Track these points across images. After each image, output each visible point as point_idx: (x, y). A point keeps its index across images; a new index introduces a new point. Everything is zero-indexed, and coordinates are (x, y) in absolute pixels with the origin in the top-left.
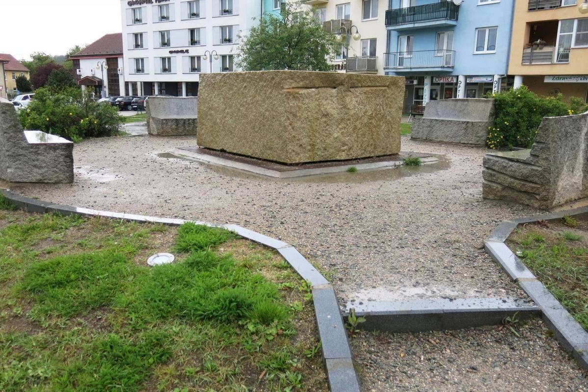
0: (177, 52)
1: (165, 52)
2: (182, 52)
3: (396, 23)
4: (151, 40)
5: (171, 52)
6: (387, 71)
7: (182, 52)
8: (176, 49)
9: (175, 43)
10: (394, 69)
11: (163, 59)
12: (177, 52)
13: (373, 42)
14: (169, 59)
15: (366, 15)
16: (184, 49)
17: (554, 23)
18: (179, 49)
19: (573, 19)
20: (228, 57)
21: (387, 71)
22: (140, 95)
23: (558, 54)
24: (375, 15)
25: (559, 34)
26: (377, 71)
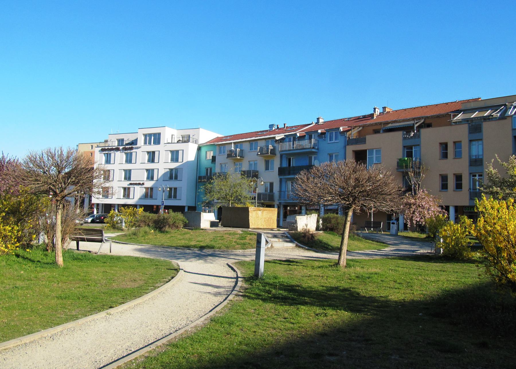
0: (136, 184)
1: (126, 184)
2: (139, 184)
3: (285, 175)
4: (118, 176)
5: (131, 184)
6: (280, 201)
7: (139, 184)
8: (135, 182)
9: (134, 178)
10: (284, 200)
11: (125, 189)
12: (136, 184)
13: (272, 184)
14: (129, 188)
15: (267, 168)
16: (141, 182)
17: (365, 151)
18: (138, 182)
19: (373, 149)
20: (157, 135)
21: (280, 201)
22: (106, 236)
23: (366, 164)
24: (272, 169)
25: (368, 156)
26: (274, 201)
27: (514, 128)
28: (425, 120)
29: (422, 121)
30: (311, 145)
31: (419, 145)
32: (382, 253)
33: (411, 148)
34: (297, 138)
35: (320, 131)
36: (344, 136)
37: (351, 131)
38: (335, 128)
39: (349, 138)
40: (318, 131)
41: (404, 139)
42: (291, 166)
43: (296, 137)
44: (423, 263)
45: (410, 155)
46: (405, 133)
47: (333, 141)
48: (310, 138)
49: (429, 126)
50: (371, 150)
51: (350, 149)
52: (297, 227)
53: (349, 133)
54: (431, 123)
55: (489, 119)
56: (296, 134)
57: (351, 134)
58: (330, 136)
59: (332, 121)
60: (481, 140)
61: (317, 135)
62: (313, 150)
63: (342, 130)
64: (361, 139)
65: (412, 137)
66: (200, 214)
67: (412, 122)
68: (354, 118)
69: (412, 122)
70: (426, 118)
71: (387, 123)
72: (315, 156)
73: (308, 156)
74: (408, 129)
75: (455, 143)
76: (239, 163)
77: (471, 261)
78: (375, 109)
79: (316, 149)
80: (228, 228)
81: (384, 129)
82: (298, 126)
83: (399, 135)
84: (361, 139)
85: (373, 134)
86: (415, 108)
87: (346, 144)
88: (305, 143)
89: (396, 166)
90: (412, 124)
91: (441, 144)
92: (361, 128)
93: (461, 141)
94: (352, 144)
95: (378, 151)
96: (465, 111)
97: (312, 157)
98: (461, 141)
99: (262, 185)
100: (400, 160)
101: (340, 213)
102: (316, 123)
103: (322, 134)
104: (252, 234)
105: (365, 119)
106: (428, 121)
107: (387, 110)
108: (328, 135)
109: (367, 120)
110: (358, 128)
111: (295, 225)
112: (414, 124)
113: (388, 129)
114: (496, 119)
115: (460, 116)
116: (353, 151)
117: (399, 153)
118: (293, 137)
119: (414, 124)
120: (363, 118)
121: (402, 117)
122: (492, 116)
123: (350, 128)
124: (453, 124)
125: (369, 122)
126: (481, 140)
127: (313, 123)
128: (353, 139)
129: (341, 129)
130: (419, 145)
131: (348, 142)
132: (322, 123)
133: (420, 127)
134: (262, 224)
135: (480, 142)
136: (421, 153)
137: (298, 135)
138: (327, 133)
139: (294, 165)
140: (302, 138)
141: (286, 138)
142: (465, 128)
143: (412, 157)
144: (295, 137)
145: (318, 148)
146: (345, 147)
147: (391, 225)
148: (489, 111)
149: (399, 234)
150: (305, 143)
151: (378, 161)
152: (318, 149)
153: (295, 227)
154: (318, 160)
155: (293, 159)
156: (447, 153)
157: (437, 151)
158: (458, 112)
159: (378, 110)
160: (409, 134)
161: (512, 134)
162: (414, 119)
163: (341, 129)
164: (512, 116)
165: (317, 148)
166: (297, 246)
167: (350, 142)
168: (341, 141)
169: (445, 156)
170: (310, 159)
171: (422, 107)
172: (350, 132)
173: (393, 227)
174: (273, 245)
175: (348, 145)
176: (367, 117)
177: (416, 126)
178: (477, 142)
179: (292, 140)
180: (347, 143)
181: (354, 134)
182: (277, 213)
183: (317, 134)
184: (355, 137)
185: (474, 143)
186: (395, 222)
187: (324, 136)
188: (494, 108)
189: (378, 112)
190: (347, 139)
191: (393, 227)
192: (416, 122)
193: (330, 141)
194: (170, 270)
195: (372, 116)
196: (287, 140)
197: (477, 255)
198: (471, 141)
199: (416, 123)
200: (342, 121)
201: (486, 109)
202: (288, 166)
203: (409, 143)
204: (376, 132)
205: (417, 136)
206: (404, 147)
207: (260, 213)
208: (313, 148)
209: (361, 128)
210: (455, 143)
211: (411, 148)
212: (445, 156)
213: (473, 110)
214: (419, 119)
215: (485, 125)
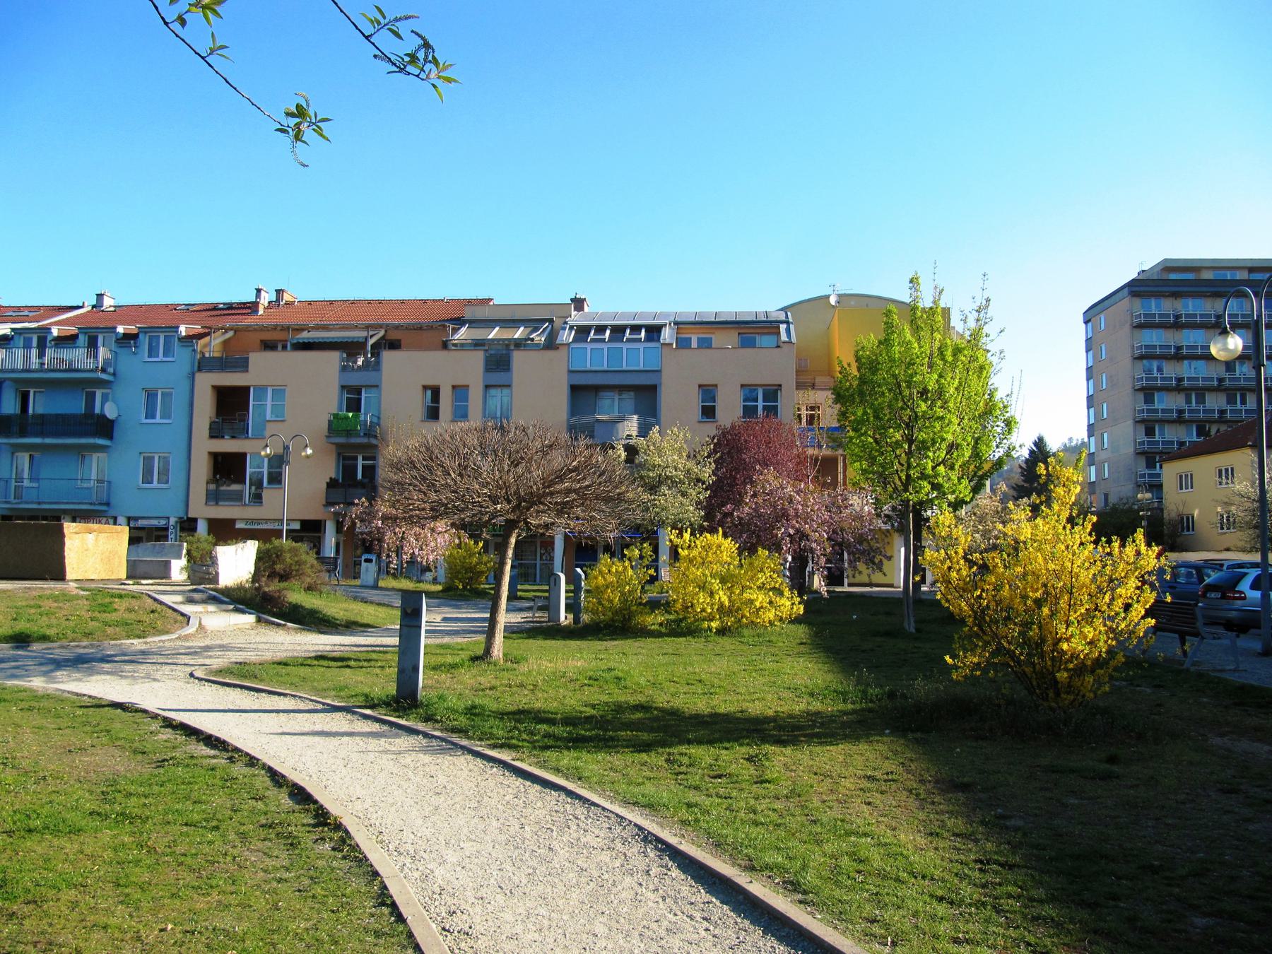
17: (246, 390)
27: (571, 369)
28: (386, 331)
29: (382, 333)
30: (98, 363)
31: (377, 386)
32: (435, 626)
33: (358, 391)
34: (53, 340)
35: (120, 329)
36: (191, 349)
37: (209, 337)
38: (166, 327)
39: (203, 354)
40: (115, 328)
41: (344, 369)
42: (31, 411)
43: (49, 338)
44: (578, 643)
45: (354, 405)
46: (345, 355)
47: (158, 357)
48: (93, 344)
49: (394, 345)
50: (262, 389)
51: (207, 382)
52: (217, 574)
53: (202, 342)
54: (400, 340)
55: (525, 345)
56: (47, 330)
57: (209, 344)
58: (150, 345)
59: (141, 306)
60: (509, 386)
61: (114, 339)
62: (104, 376)
63: (184, 334)
64: (232, 360)
65: (359, 367)
66: (60, 536)
67: (364, 334)
68: (203, 307)
69: (364, 334)
70: (388, 328)
71: (300, 329)
72: (105, 391)
73: (83, 389)
74: (351, 348)
75: (454, 387)
76: (1242, 382)
77: (644, 633)
78: (259, 291)
79: (109, 374)
80: (17, 582)
81: (295, 341)
82: (39, 308)
83: (335, 357)
84: (232, 360)
85: (260, 350)
86: (353, 302)
87: (196, 368)
88: (78, 356)
89: (327, 430)
90: (363, 337)
91: (425, 388)
92: (231, 334)
93: (468, 386)
94: (210, 370)
95: (279, 392)
96: (473, 323)
97: (94, 393)
98: (468, 386)
99: (308, 457)
100: (336, 416)
101: (173, 536)
102: (94, 307)
103: (127, 337)
104: (126, 596)
105: (230, 312)
106: (393, 335)
107: (287, 297)
108: (144, 340)
109: (242, 314)
110: (223, 334)
111: (211, 570)
112: (366, 338)
113: (299, 343)
114: (537, 347)
115: (463, 334)
116: (214, 387)
117: (329, 402)
118: (39, 337)
119: (366, 338)
120: (228, 309)
121: (330, 318)
122: (533, 340)
123: (206, 330)
124: (453, 348)
125: (249, 321)
126: (509, 386)
127: (86, 304)
128: (214, 357)
129: (183, 330)
130: (377, 386)
131: (199, 363)
132: (112, 309)
133: (377, 348)
134: (96, 569)
135: (506, 391)
136: (382, 406)
137: (55, 332)
138: (141, 336)
139: (40, 411)
140: (67, 341)
141: (16, 338)
142: (478, 357)
143: (359, 410)
144: (46, 338)
145: (114, 370)
146: (193, 374)
147: (364, 564)
148: (522, 329)
149: (381, 584)
150: (78, 356)
151: (277, 416)
152: (114, 374)
153: (210, 574)
154: (114, 402)
155: (37, 394)
156: (437, 408)
157: (417, 403)
158: (460, 322)
159: (266, 295)
160: (353, 359)
161: (568, 382)
162: (367, 327)
163: (183, 330)
164: (568, 345)
165: (111, 370)
166: (259, 620)
167: (204, 364)
168: (182, 359)
169: (433, 413)
170: (91, 398)
171: (369, 302)
172: (207, 339)
173: (367, 570)
174: (203, 623)
175: (200, 370)
176: (235, 308)
177: (371, 342)
178: (499, 390)
179: (35, 343)
180: (199, 367)
181: (213, 345)
182: (127, 538)
183: (114, 335)
184: (217, 355)
185: (493, 392)
186: (374, 559)
187: (135, 343)
188: (534, 324)
189: (265, 299)
190: (198, 356)
191: (367, 570)
192: (371, 333)
193: (165, 355)
194: (274, 715)
195: (252, 307)
196: (20, 341)
197: (654, 620)
198: (487, 387)
199: (372, 336)
200: (190, 311)
201: (513, 323)
202: (18, 411)
203: (354, 380)
204: (269, 346)
205: (374, 366)
206: (343, 387)
207: (91, 537)
208: (104, 370)
209: (231, 334)
210: (454, 387)
211: (358, 391)
212: (433, 413)
213: (490, 323)
214: (377, 327)
215: (518, 357)
